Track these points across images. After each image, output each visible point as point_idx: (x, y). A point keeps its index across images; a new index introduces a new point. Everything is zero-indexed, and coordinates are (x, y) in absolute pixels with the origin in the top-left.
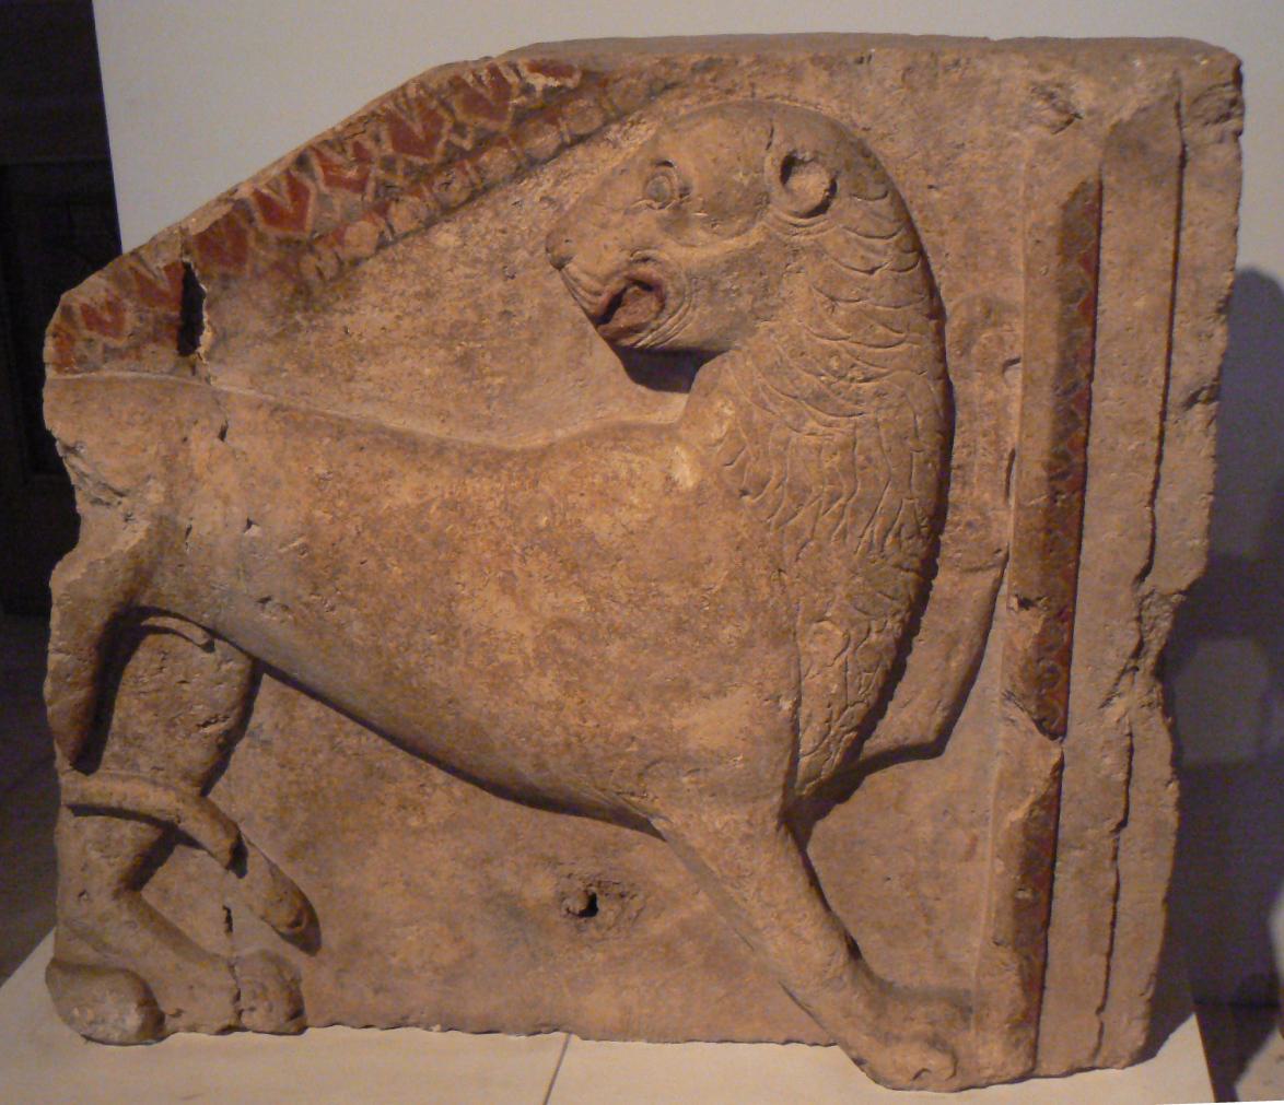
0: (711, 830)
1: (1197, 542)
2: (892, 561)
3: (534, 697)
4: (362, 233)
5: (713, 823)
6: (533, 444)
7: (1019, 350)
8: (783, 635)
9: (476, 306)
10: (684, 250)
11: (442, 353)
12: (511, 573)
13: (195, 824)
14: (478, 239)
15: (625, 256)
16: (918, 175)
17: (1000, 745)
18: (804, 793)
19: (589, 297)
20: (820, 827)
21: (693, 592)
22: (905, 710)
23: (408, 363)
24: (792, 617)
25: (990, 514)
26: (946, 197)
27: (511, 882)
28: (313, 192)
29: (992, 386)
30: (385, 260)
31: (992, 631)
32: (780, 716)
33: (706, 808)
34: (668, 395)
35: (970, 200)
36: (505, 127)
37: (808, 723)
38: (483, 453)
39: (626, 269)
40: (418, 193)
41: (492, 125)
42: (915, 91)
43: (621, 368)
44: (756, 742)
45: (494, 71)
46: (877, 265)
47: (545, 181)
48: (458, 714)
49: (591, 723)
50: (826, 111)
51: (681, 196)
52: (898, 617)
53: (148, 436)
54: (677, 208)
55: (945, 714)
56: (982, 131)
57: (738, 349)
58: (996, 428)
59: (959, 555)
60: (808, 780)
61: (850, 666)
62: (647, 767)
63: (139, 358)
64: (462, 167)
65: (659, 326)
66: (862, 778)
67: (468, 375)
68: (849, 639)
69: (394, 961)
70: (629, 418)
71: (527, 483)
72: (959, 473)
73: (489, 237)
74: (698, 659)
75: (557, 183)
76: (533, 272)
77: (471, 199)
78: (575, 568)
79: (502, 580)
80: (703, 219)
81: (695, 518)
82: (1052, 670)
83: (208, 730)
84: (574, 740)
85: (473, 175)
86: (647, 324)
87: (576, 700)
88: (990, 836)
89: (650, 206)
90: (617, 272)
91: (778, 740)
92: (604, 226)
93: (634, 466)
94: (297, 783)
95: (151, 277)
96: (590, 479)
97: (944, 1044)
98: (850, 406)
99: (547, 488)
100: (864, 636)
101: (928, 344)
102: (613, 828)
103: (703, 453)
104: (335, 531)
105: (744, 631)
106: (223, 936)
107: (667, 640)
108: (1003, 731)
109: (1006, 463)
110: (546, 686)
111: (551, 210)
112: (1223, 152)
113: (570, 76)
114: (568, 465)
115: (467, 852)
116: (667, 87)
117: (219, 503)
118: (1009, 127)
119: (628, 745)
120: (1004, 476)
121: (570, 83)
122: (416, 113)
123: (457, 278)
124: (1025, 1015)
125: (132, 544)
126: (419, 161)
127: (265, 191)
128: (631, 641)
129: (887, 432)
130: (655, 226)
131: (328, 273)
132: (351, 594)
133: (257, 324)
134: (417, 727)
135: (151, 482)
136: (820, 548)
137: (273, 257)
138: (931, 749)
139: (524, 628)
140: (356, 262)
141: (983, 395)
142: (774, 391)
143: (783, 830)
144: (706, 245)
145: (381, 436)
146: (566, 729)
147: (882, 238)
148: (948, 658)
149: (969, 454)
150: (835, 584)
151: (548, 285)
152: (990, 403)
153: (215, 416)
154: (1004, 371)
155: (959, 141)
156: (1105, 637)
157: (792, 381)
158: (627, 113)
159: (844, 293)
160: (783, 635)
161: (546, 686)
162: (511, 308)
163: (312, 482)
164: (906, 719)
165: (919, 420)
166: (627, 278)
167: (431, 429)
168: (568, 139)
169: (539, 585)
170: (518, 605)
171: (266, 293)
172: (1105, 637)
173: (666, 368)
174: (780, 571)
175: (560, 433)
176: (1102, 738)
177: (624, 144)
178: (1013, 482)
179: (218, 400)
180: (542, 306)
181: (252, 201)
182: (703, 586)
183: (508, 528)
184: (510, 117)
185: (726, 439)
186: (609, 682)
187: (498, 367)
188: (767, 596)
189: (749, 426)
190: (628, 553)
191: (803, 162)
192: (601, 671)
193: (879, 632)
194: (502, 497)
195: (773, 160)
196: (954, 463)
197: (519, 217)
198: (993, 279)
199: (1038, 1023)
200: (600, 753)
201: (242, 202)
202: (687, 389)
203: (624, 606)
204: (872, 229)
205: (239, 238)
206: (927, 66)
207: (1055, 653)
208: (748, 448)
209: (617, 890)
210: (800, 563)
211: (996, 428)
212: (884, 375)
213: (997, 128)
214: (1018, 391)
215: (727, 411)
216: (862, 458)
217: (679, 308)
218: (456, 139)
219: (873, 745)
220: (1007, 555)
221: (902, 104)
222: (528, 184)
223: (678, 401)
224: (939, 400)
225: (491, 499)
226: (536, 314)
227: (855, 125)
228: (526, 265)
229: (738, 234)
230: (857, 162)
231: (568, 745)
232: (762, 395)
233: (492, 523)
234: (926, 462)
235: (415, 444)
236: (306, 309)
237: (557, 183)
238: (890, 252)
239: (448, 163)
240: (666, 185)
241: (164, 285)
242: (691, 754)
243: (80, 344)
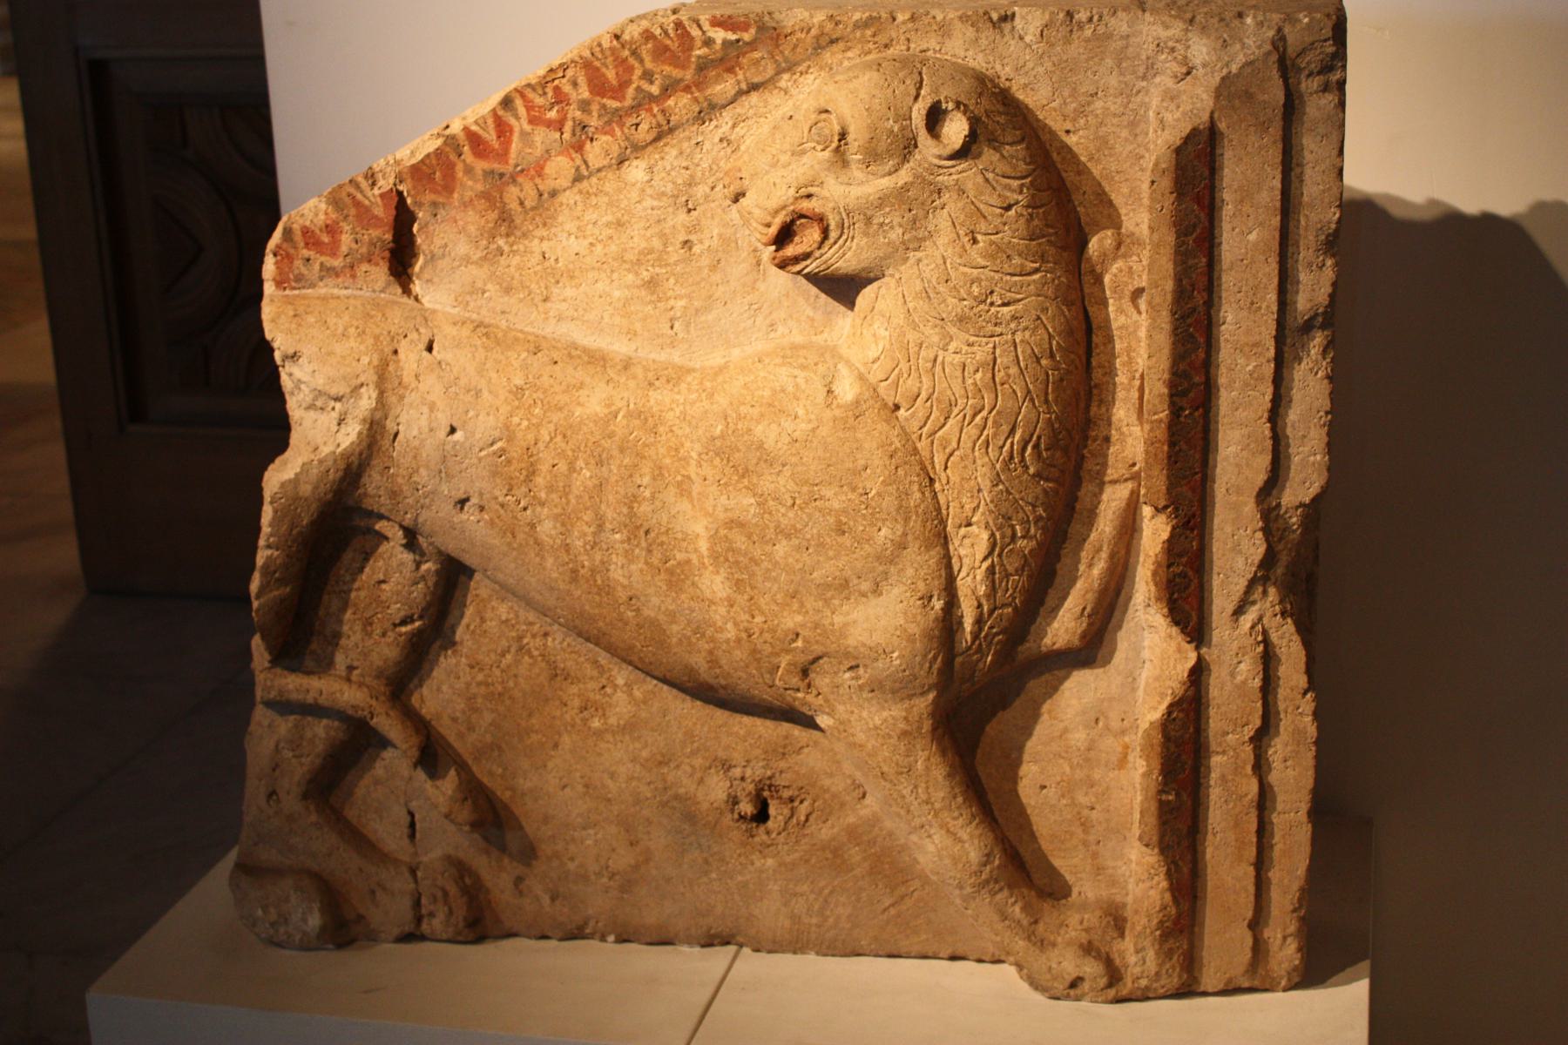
1: (1318, 457)
4: (560, 168)
9: (662, 235)
11: (631, 277)
12: (689, 477)
13: (388, 724)
21: (851, 496)
23: (600, 285)
27: (687, 786)
28: (517, 129)
30: (580, 192)
36: (689, 75)
40: (611, 133)
41: (677, 73)
45: (679, 25)
48: (638, 610)
49: (759, 619)
50: (972, 64)
53: (362, 348)
56: (1113, 81)
57: (892, 276)
63: (354, 276)
64: (650, 110)
66: (1306, 644)
67: (654, 297)
69: (571, 866)
78: (746, 473)
82: (1183, 575)
83: (404, 629)
84: (744, 635)
85: (660, 118)
90: (784, 207)
94: (487, 685)
95: (367, 202)
97: (1098, 952)
98: (990, 328)
104: (531, 437)
106: (406, 841)
112: (1329, 99)
113: (746, 30)
115: (645, 754)
116: (832, 42)
117: (425, 410)
119: (794, 641)
121: (747, 37)
122: (610, 59)
123: (645, 209)
124: (1177, 922)
125: (343, 446)
126: (613, 104)
127: (474, 128)
131: (528, 204)
132: (543, 495)
133: (462, 248)
134: (601, 624)
135: (363, 390)
137: (480, 187)
140: (554, 194)
145: (574, 353)
146: (736, 624)
153: (422, 330)
155: (1092, 90)
156: (1236, 547)
158: (796, 64)
161: (715, 584)
163: (510, 392)
164: (1063, 627)
167: (620, 347)
169: (714, 488)
171: (473, 221)
172: (1236, 547)
176: (1235, 645)
177: (793, 91)
179: (426, 317)
181: (462, 137)
186: (775, 580)
187: (679, 290)
190: (794, 460)
192: (768, 570)
199: (1192, 933)
200: (768, 649)
201: (453, 137)
205: (449, 169)
207: (1184, 560)
209: (786, 794)
218: (646, 86)
222: (709, 127)
229: (890, 174)
235: (604, 359)
236: (508, 235)
237: (734, 126)
239: (636, 108)
241: (379, 211)
243: (298, 263)
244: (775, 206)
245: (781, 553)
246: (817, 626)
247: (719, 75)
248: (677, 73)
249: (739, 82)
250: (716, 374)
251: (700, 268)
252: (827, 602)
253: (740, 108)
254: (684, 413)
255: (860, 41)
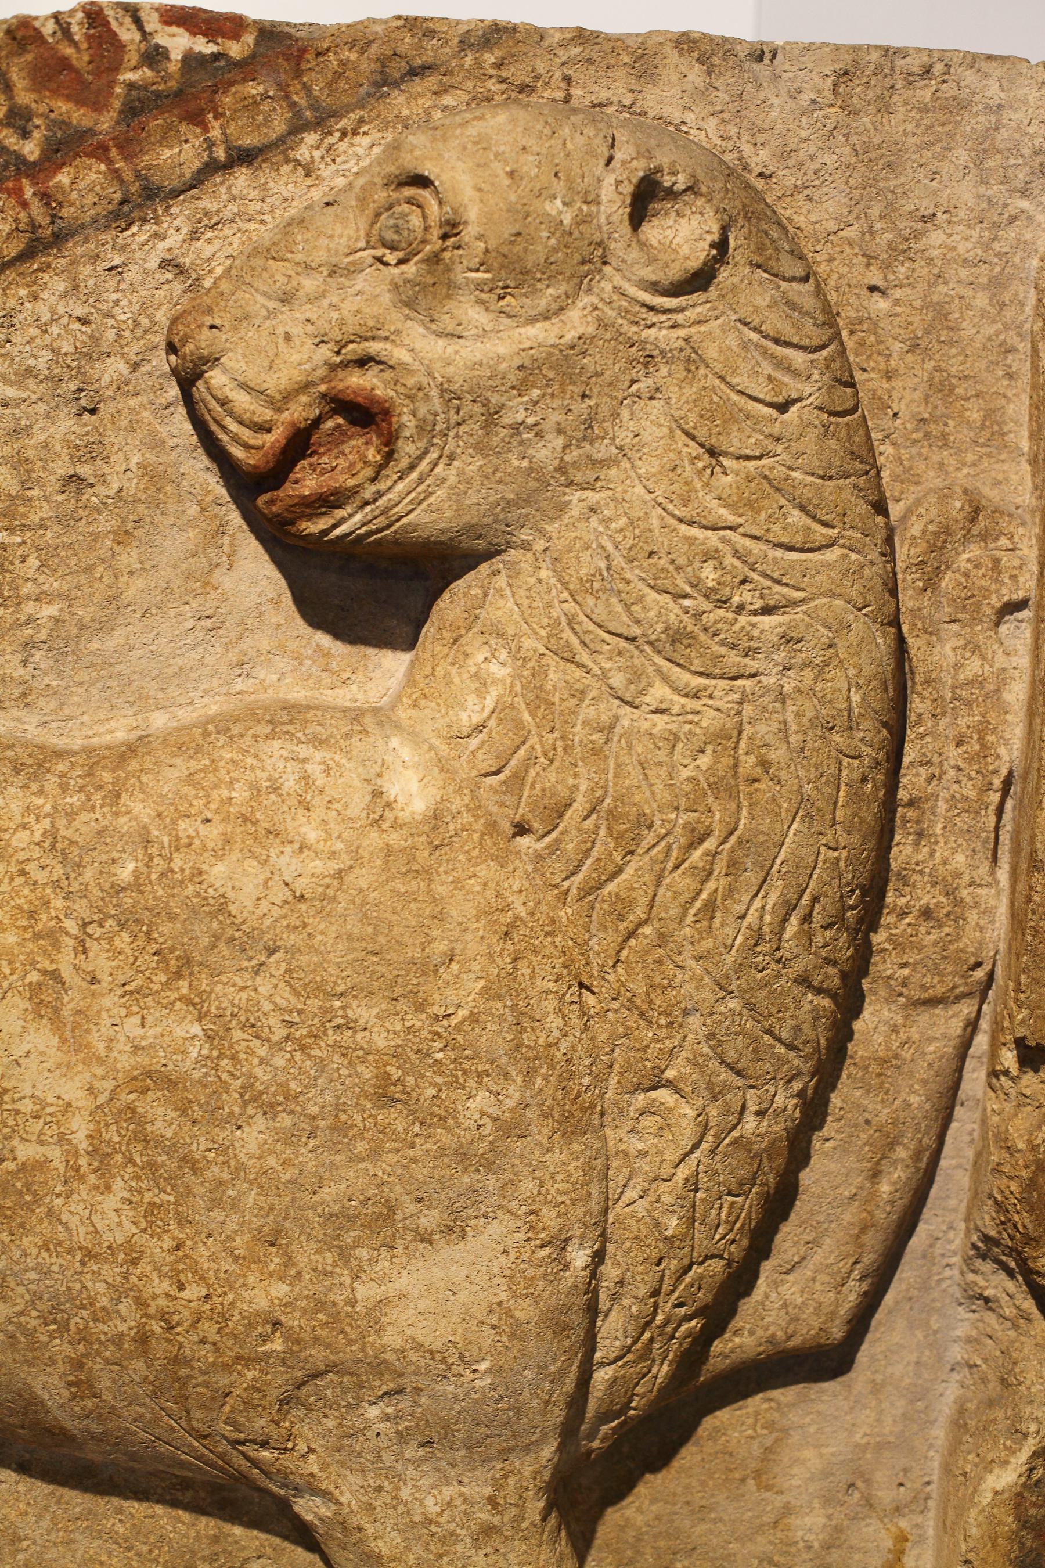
0: (417, 1518)
2: (795, 970)
3: (82, 1235)
5: (421, 1502)
6: (107, 739)
7: (1027, 585)
8: (578, 1117)
10: (441, 342)
12: (55, 976)
14: (33, 331)
15: (325, 352)
16: (851, 266)
17: (957, 1353)
18: (596, 1444)
19: (245, 434)
20: (612, 1516)
21: (414, 1020)
22: (791, 1278)
24: (600, 1080)
25: (964, 893)
26: (898, 309)
29: (976, 649)
31: (954, 1125)
32: (569, 1279)
33: (410, 1473)
34: (371, 651)
35: (941, 313)
36: (106, 122)
37: (615, 1298)
38: (11, 747)
39: (322, 380)
41: (79, 116)
42: (854, 113)
43: (287, 598)
44: (517, 1333)
46: (794, 395)
47: (171, 231)
49: (193, 1292)
51: (445, 237)
52: (797, 1086)
54: (435, 259)
55: (865, 1287)
56: (966, 194)
57: (526, 546)
58: (983, 729)
59: (906, 972)
60: (604, 1417)
61: (703, 1178)
62: (299, 1387)
64: (18, 192)
65: (379, 494)
66: (697, 1423)
68: (706, 1128)
70: (298, 694)
71: (98, 797)
72: (911, 814)
73: (55, 330)
74: (414, 1160)
75: (194, 236)
76: (133, 402)
77: (26, 255)
79: (35, 990)
80: (479, 286)
81: (426, 873)
85: (37, 209)
86: (355, 491)
87: (167, 1243)
88: (931, 1532)
89: (380, 260)
91: (562, 1329)
92: (286, 299)
93: (314, 769)
96: (225, 793)
98: (733, 658)
99: (140, 809)
100: (732, 1119)
101: (873, 555)
102: (207, 1525)
103: (444, 749)
105: (509, 1103)
107: (358, 1118)
108: (964, 1322)
109: (995, 797)
110: (108, 1213)
111: (178, 287)
113: (237, 37)
114: (182, 766)
116: (414, 72)
118: (1013, 191)
119: (265, 1338)
120: (993, 819)
121: (235, 50)
128: (286, 1120)
129: (797, 714)
130: (387, 298)
136: (663, 939)
138: (824, 1361)
139: (73, 1090)
141: (958, 666)
142: (591, 627)
143: (553, 1520)
144: (483, 334)
146: (140, 1302)
147: (803, 348)
148: (875, 1175)
149: (929, 780)
150: (686, 1012)
151: (163, 430)
152: (969, 683)
154: (997, 624)
155: (926, 207)
157: (627, 607)
158: (335, 114)
159: (734, 441)
160: (578, 1117)
161: (108, 1213)
162: (85, 470)
164: (790, 1299)
165: (856, 698)
166: (324, 396)
168: (220, 154)
170: (64, 1041)
173: (373, 589)
174: (581, 985)
175: (159, 721)
177: (327, 171)
178: (1005, 838)
180: (143, 466)
182: (435, 1009)
183: (56, 885)
184: (117, 104)
185: (492, 723)
186: (234, 1204)
188: (556, 1033)
189: (539, 700)
190: (293, 939)
191: (671, 194)
192: (222, 1183)
193: (761, 1113)
194: (46, 823)
195: (618, 183)
196: (902, 794)
197: (114, 296)
198: (974, 465)
202: (410, 644)
203: (279, 1046)
204: (789, 333)
206: (878, 71)
208: (533, 740)
210: (620, 970)
211: (983, 729)
212: (797, 603)
213: (994, 190)
214: (1024, 661)
215: (494, 668)
216: (752, 760)
217: (420, 458)
219: (742, 1340)
220: (991, 976)
221: (831, 135)
222: (138, 234)
223: (391, 666)
224: (889, 665)
225: (24, 826)
226: (132, 484)
227: (746, 168)
228: (121, 387)
230: (753, 223)
231: (143, 1339)
232: (567, 634)
233: (23, 873)
234: (864, 780)
237: (194, 236)
238: (816, 376)
240: (415, 221)
242: (388, 1356)
244: (284, 383)
245: (252, 1147)
246: (320, 1305)
247: (170, 127)
248: (79, 116)
249: (210, 144)
250: (122, 757)
251: (96, 537)
252: (344, 1254)
253: (211, 200)
254: (52, 834)
255: (470, 74)
